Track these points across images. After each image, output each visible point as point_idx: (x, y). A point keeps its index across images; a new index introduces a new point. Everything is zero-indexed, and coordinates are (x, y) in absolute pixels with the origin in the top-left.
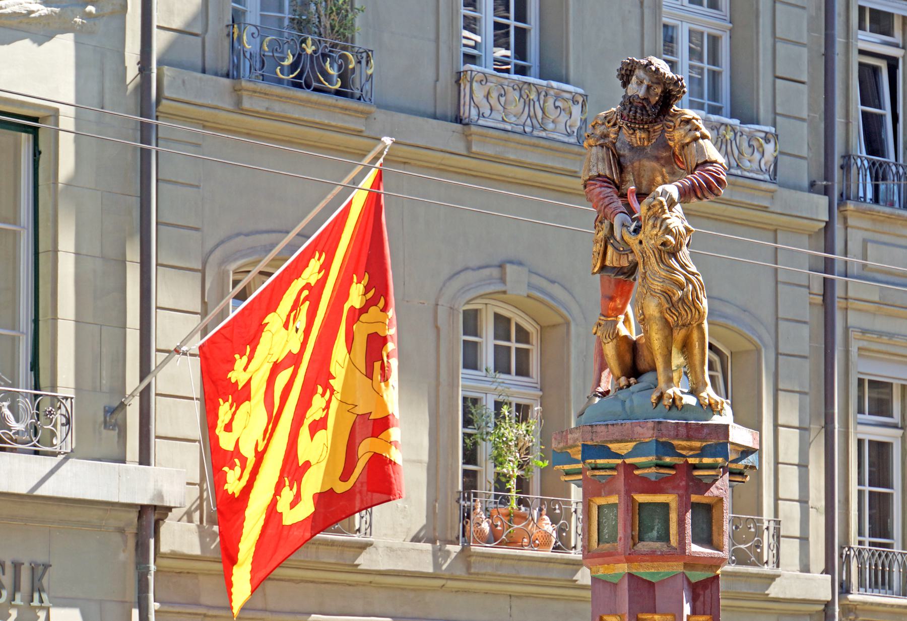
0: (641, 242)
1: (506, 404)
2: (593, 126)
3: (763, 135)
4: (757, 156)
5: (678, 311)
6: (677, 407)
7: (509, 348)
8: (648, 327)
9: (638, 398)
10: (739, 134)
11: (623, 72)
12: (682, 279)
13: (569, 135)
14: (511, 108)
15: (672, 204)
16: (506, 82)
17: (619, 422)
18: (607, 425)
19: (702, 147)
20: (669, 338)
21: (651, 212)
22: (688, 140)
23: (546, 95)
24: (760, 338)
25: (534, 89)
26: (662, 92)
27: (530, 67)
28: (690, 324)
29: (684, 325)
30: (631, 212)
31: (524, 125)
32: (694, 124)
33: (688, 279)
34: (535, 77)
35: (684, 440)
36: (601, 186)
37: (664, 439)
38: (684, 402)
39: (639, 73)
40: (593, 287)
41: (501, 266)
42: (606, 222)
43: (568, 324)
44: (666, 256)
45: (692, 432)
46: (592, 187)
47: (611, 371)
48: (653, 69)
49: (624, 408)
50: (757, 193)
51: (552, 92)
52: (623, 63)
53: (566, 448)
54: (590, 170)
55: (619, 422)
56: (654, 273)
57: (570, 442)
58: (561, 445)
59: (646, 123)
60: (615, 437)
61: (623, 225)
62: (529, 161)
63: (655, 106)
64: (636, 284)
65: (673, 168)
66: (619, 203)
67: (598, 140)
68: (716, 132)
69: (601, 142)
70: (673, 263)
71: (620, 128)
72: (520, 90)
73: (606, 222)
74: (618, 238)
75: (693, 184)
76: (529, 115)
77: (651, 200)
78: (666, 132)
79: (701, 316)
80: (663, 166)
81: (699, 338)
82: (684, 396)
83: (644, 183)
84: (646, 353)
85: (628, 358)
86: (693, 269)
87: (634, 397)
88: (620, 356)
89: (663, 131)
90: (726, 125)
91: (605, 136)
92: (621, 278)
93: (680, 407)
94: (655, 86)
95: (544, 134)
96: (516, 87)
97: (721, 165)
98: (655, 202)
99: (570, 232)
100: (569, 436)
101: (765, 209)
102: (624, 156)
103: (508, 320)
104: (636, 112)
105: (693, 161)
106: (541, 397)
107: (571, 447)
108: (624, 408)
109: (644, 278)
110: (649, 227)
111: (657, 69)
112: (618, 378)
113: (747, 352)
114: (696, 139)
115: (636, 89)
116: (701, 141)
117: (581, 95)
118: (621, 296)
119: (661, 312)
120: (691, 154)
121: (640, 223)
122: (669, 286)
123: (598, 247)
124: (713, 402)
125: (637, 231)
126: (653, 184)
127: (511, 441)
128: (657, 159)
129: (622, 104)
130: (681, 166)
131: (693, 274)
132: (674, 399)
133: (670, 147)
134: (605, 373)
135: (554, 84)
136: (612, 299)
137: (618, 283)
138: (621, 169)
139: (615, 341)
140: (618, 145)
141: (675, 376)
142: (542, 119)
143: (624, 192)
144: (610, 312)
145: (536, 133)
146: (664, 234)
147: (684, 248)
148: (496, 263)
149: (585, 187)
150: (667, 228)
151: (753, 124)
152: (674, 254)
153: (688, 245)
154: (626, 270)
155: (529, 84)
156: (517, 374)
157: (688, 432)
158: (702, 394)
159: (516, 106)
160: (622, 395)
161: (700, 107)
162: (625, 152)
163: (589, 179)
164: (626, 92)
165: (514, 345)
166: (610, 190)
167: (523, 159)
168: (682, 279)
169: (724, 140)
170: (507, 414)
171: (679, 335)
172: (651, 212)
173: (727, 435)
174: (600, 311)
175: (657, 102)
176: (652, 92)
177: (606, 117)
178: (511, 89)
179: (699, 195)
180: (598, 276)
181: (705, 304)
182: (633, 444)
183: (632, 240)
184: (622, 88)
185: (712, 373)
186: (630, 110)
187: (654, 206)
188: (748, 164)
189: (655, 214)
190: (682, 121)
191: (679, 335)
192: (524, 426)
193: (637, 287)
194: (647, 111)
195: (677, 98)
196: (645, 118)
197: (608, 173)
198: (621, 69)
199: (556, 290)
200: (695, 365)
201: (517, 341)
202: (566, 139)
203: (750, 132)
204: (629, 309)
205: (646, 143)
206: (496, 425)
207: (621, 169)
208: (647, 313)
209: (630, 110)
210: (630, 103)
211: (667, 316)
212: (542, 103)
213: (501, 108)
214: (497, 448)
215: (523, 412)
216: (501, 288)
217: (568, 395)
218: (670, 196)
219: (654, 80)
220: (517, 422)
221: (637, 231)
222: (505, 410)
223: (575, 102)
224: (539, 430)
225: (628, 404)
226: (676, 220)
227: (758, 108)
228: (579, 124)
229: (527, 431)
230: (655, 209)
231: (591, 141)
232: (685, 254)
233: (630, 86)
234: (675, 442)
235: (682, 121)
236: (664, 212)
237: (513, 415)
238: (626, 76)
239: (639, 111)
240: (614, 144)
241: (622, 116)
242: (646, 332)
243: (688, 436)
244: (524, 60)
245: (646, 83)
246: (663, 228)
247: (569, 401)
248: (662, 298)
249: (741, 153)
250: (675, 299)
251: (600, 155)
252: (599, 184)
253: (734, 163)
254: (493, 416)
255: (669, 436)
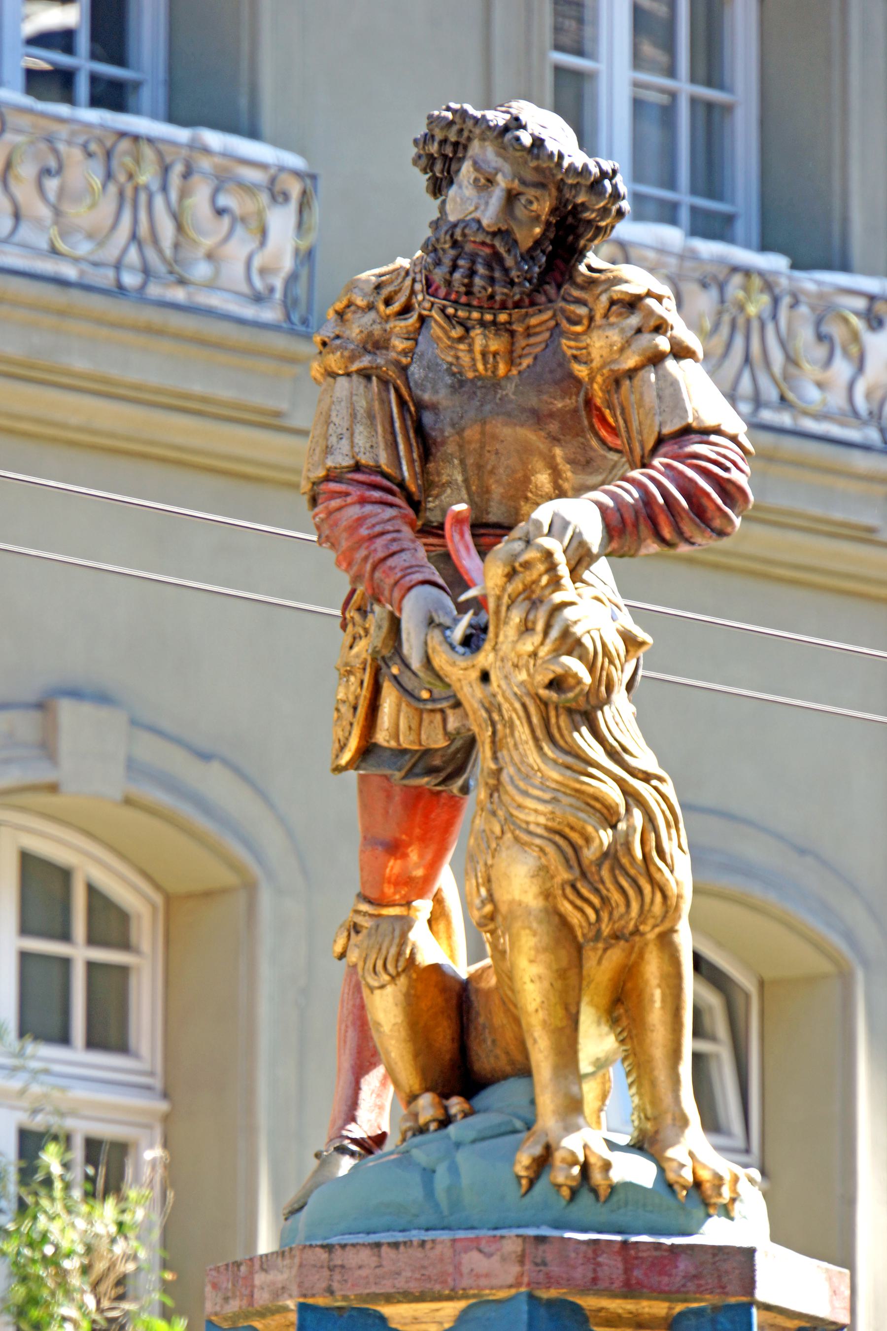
0: (485, 677)
1: (55, 1138)
2: (340, 314)
3: (860, 304)
4: (842, 369)
5: (600, 899)
6: (594, 1191)
7: (65, 963)
8: (505, 941)
9: (476, 1163)
10: (786, 301)
11: (434, 148)
12: (614, 794)
13: (258, 299)
14: (79, 214)
15: (581, 558)
16: (63, 131)
17: (416, 1235)
18: (378, 1245)
19: (674, 384)
20: (572, 974)
21: (516, 585)
22: (631, 361)
23: (187, 174)
24: (849, 936)
25: (148, 152)
26: (553, 211)
27: (137, 85)
28: (636, 932)
29: (616, 936)
30: (457, 581)
31: (118, 266)
32: (651, 313)
33: (629, 793)
34: (154, 116)
35: (613, 1296)
36: (363, 501)
37: (553, 1293)
38: (617, 1176)
39: (483, 151)
40: (338, 805)
41: (42, 706)
42: (379, 612)
43: (251, 888)
44: (564, 721)
45: (642, 1271)
46: (335, 503)
47: (391, 1074)
48: (527, 141)
49: (429, 1192)
50: (841, 484)
51: (205, 164)
52: (432, 120)
53: (247, 1316)
54: (328, 450)
55: (416, 1235)
56: (527, 775)
57: (262, 1298)
58: (234, 1306)
59: (503, 307)
60: (401, 1283)
61: (431, 622)
62: (133, 376)
63: (529, 256)
64: (470, 803)
65: (585, 447)
66: (418, 552)
67: (352, 359)
68: (714, 292)
69: (365, 362)
70: (584, 740)
71: (422, 319)
72: (109, 155)
73: (379, 612)
74: (416, 663)
75: (647, 498)
76: (134, 236)
77: (518, 546)
78: (563, 333)
79: (670, 909)
80: (555, 440)
81: (664, 977)
82: (616, 1158)
83: (497, 491)
84: (500, 1019)
85: (444, 1036)
86: (644, 758)
87: (461, 1157)
88: (417, 1029)
89: (556, 331)
90: (747, 272)
91: (376, 344)
92: (422, 788)
93: (603, 1192)
94: (531, 193)
95: (179, 295)
96: (93, 147)
97: (734, 439)
98: (531, 554)
99: (257, 617)
100: (259, 1279)
101: (865, 535)
102: (434, 408)
103: (65, 875)
104: (472, 273)
105: (650, 424)
106: (166, 1119)
107: (263, 1314)
108: (429, 1192)
109: (495, 789)
110: (509, 632)
111: (538, 142)
112: (412, 1098)
113: (811, 980)
114: (656, 359)
115: (471, 202)
116: (670, 364)
117: (297, 174)
118: (423, 840)
119: (547, 895)
120: (640, 404)
121: (483, 618)
122: (569, 814)
123: (353, 689)
124: (705, 1175)
125: (472, 642)
126: (522, 495)
127: (68, 1256)
128: (538, 418)
129: (431, 248)
130: (609, 439)
131: (647, 777)
132: (585, 1168)
133: (578, 381)
134: (372, 1081)
135: (213, 139)
136: (395, 849)
137: (415, 800)
138: (426, 446)
139: (403, 980)
140: (416, 371)
141: (590, 1091)
142: (176, 246)
143: (434, 517)
144: (389, 890)
145: (154, 290)
146: (557, 652)
147: (620, 695)
148: (31, 696)
149: (314, 501)
150: (566, 633)
151: (828, 266)
152: (586, 715)
153: (629, 687)
154: (437, 762)
155: (136, 138)
156: (93, 1043)
157: (627, 1271)
158: (670, 1153)
159: (95, 210)
160: (424, 1152)
161: (668, 214)
162: (436, 394)
163: (327, 479)
164: (442, 208)
165: (80, 953)
166: (390, 512)
167: (114, 373)
168: (614, 794)
169: (741, 321)
170: (56, 1169)
171: (601, 968)
172: (516, 585)
173: (749, 1284)
174: (357, 888)
175: (537, 243)
176: (520, 211)
177: (378, 287)
178: (77, 154)
179: (667, 533)
180: (352, 775)
181: (680, 875)
182: (461, 1305)
183: (459, 671)
184: (429, 198)
185: (705, 1047)
186: (454, 267)
187: (527, 565)
188: (813, 394)
189: (528, 588)
190: (612, 303)
191: (601, 968)
192: (109, 1209)
193: (472, 816)
194: (506, 271)
195: (600, 231)
196: (500, 291)
197: (383, 460)
198: (428, 138)
199: (216, 783)
200: (650, 1060)
201: (92, 940)
202: (249, 312)
203: (821, 296)
204: (446, 880)
205: (502, 369)
206: (22, 1206)
207: (426, 446)
208: (503, 896)
209: (454, 267)
210: (455, 244)
211: (566, 907)
212: (174, 195)
213: (45, 212)
214: (24, 1279)
215: (106, 1166)
216: (43, 774)
217: (250, 1110)
218: (577, 535)
219: (530, 176)
220: (90, 1195)
221: (472, 642)
222: (51, 1158)
223: (279, 196)
224: (157, 1219)
225: (442, 1180)
226: (597, 607)
227: (845, 220)
228: (287, 264)
229: (120, 1225)
230: (530, 576)
231: (334, 361)
232: (620, 716)
233: (453, 191)
234: (589, 1302)
235: (612, 303)
236: (556, 584)
237: (77, 1175)
238: (443, 156)
239: (481, 270)
240: (404, 369)
241: (429, 283)
242: (500, 954)
243: (627, 1284)
244: (120, 60)
245: (502, 182)
246: (554, 633)
247: (251, 1131)
248: (550, 849)
249: (791, 360)
250: (590, 854)
251: (361, 404)
252: (356, 492)
253: (770, 393)
254: (13, 1176)
255: (569, 1282)
